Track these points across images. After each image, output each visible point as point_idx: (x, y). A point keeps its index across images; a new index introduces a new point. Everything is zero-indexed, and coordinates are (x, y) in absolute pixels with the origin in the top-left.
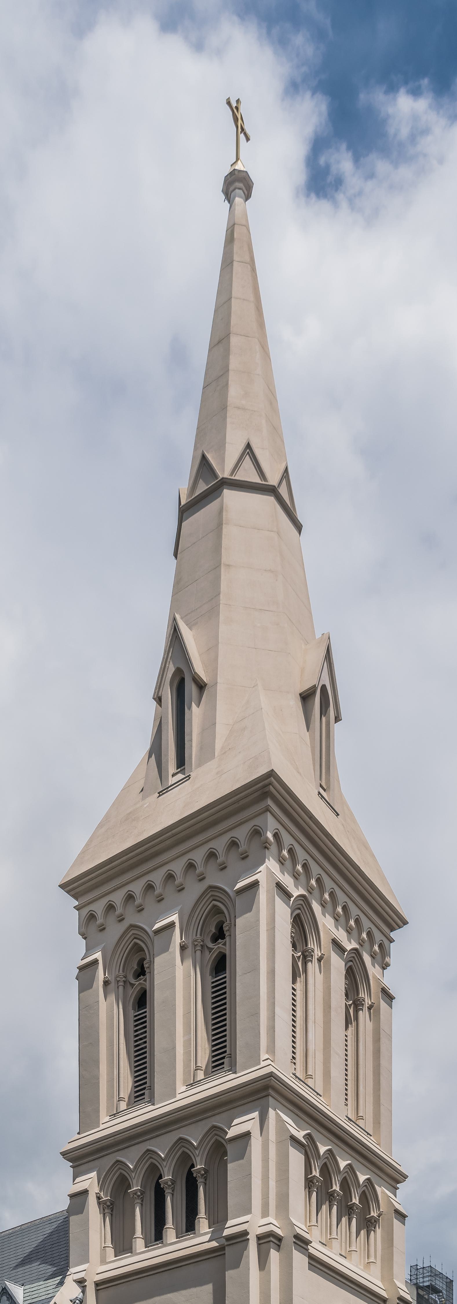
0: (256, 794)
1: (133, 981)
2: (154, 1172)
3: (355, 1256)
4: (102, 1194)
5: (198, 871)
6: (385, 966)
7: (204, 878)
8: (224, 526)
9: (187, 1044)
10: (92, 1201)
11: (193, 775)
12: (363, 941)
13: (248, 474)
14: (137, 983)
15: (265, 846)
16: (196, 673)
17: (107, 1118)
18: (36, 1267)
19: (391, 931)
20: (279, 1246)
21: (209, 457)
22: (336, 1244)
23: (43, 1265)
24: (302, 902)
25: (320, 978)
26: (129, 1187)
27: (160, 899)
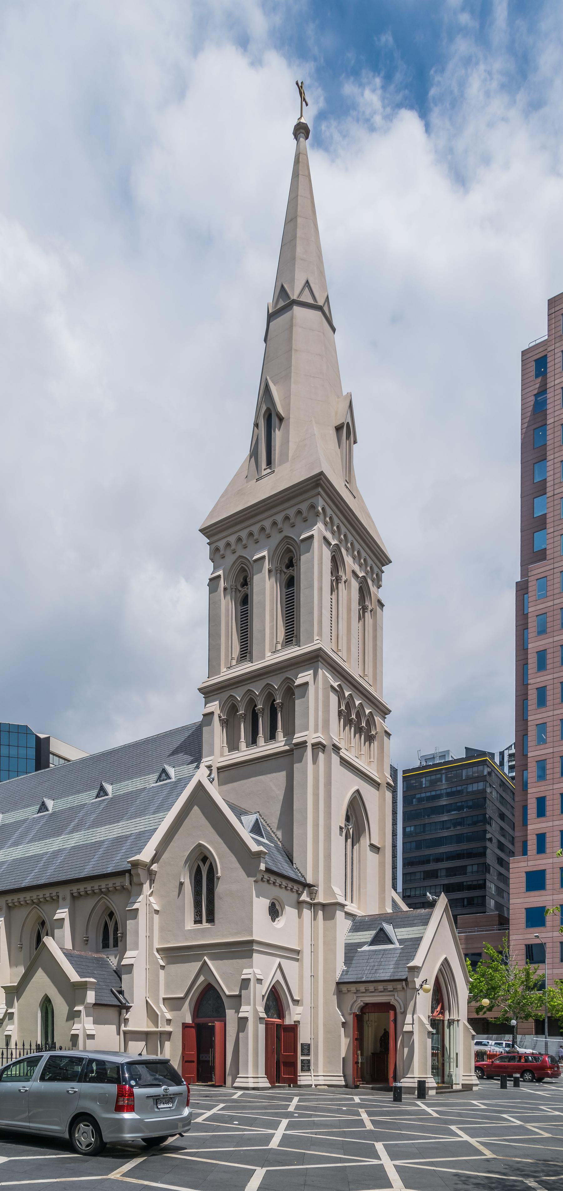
0: (312, 485)
1: (240, 589)
2: (252, 704)
3: (363, 757)
4: (221, 714)
5: (279, 527)
6: (379, 587)
7: (282, 531)
8: (294, 327)
9: (271, 628)
10: (216, 719)
11: (276, 470)
12: (368, 571)
13: (307, 298)
14: (243, 590)
15: (317, 515)
16: (278, 411)
17: (225, 670)
18: (181, 757)
19: (383, 566)
20: (324, 750)
21: (286, 286)
22: (353, 750)
23: (186, 755)
24: (336, 548)
25: (345, 592)
26: (237, 711)
27: (257, 542)
